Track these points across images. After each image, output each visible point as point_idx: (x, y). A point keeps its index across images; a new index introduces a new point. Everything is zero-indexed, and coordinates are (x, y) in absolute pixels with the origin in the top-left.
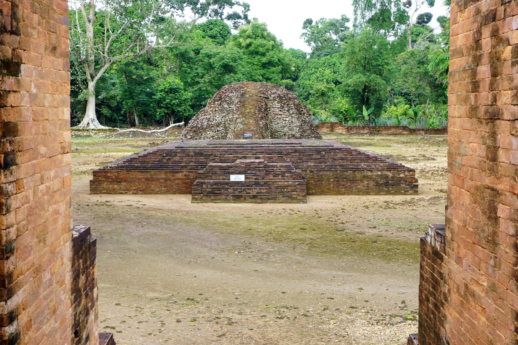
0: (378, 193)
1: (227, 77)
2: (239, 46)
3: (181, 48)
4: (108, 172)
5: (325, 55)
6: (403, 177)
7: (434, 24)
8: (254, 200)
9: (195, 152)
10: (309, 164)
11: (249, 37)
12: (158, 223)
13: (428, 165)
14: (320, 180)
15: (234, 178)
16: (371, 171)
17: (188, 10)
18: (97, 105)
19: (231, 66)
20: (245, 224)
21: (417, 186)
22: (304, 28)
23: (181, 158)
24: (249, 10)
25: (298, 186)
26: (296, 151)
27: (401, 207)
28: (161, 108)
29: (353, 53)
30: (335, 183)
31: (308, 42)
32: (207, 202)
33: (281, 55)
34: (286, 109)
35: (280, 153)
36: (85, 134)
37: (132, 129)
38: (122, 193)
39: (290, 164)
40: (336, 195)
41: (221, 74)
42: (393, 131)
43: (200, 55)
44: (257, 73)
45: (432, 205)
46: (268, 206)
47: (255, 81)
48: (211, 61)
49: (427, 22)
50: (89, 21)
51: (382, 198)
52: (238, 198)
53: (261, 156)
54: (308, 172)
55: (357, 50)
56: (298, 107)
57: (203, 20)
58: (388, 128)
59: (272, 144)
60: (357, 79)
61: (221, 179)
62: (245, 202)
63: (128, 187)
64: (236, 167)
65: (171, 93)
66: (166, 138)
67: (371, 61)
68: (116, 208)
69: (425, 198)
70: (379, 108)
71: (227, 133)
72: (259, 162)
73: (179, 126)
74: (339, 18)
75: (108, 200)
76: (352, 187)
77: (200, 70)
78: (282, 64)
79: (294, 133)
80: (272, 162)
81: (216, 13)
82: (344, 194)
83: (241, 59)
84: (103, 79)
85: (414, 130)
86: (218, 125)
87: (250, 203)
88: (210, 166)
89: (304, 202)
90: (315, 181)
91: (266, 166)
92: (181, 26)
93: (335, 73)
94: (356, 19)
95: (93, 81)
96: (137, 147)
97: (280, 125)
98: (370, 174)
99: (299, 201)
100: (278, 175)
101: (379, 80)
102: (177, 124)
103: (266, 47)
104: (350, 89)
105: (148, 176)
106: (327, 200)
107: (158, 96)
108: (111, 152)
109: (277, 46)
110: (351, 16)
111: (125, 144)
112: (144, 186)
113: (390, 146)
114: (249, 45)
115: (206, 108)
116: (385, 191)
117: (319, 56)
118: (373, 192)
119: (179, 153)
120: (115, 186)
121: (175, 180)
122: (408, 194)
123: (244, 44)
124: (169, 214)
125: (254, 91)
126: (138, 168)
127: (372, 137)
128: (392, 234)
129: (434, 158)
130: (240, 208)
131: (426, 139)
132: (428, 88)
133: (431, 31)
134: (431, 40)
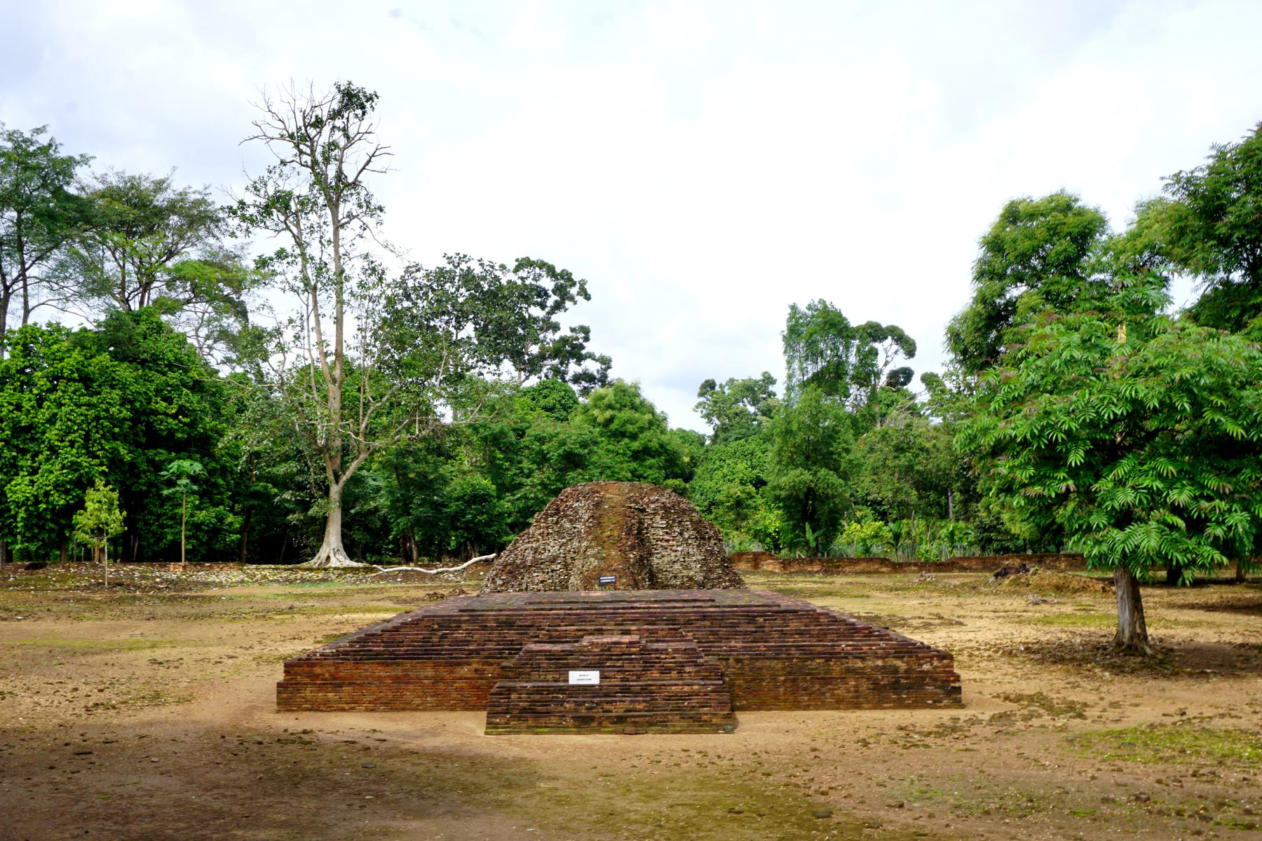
0: (878, 706)
1: (572, 474)
2: (594, 421)
3: (493, 426)
4: (313, 665)
5: (737, 439)
6: (928, 672)
7: (915, 386)
8: (619, 727)
9: (497, 621)
10: (733, 644)
11: (610, 407)
12: (399, 796)
13: (956, 636)
14: (757, 678)
15: (576, 677)
16: (863, 659)
17: (507, 365)
18: (343, 525)
19: (578, 455)
20: (597, 795)
21: (958, 690)
22: (701, 395)
23: (469, 632)
24: (609, 367)
25: (713, 696)
26: (704, 617)
27: (939, 741)
28: (456, 529)
29: (788, 432)
30: (788, 684)
31: (708, 417)
32: (519, 733)
33: (664, 438)
34: (677, 529)
35: (672, 621)
36: (321, 575)
37: (404, 568)
38: (343, 710)
39: (694, 645)
40: (790, 709)
41: (560, 470)
42: (862, 566)
43: (526, 438)
44: (622, 469)
45: (1003, 737)
46: (650, 743)
47: (619, 480)
48: (544, 447)
49: (904, 384)
50: (334, 381)
51: (891, 718)
52: (584, 723)
53: (633, 628)
54: (731, 661)
55: (795, 427)
56: (697, 525)
57: (533, 381)
58: (854, 561)
59: (656, 602)
60: (797, 476)
61: (549, 679)
62: (600, 733)
63: (357, 695)
64: (581, 653)
65: (474, 503)
66: (458, 585)
67: (818, 450)
68: (320, 750)
69: (981, 717)
70: (833, 527)
71: (569, 575)
72: (631, 643)
73: (486, 561)
74: (759, 377)
75: (308, 728)
76: (824, 694)
77: (526, 464)
78: (666, 451)
79: (691, 573)
80: (658, 641)
81: (556, 371)
82: (807, 708)
83: (596, 443)
84: (356, 480)
85: (901, 565)
86: (553, 560)
87: (610, 733)
88: (527, 652)
89: (727, 732)
90: (746, 682)
91: (644, 650)
92: (494, 387)
93: (753, 468)
94: (790, 377)
95: (337, 482)
96: (405, 601)
97: (666, 559)
98: (860, 664)
99: (715, 729)
100: (670, 670)
101: (834, 479)
102: (484, 557)
103: (639, 424)
104: (783, 493)
105: (398, 672)
106: (774, 725)
107: (453, 507)
108: (355, 611)
109: (657, 422)
110: (780, 373)
111: (386, 594)
112: (390, 695)
113: (868, 597)
114: (611, 420)
115: (531, 530)
116: (894, 701)
117: (726, 440)
118: (869, 702)
119: (465, 622)
120: (330, 695)
121: (455, 680)
122: (940, 708)
123: (600, 419)
124: (432, 766)
125: (617, 499)
126: (377, 655)
127: (829, 579)
128: (948, 826)
129: (961, 620)
130: (590, 747)
131: (930, 583)
132: (914, 492)
133: (913, 397)
134: (914, 411)
